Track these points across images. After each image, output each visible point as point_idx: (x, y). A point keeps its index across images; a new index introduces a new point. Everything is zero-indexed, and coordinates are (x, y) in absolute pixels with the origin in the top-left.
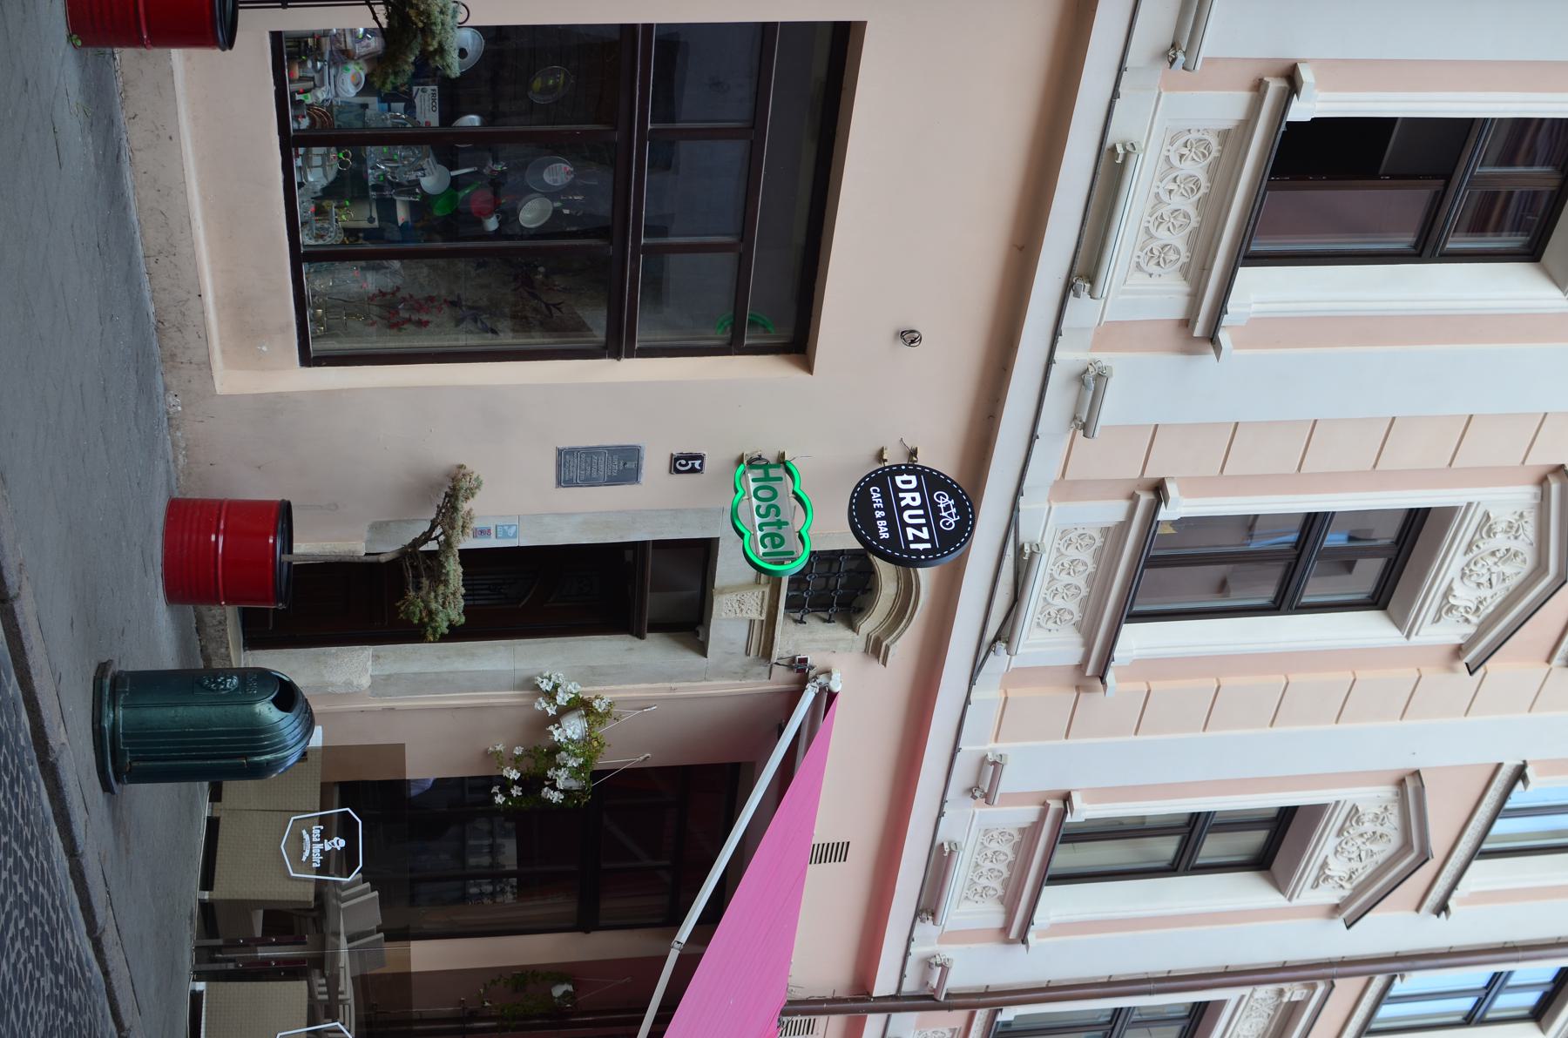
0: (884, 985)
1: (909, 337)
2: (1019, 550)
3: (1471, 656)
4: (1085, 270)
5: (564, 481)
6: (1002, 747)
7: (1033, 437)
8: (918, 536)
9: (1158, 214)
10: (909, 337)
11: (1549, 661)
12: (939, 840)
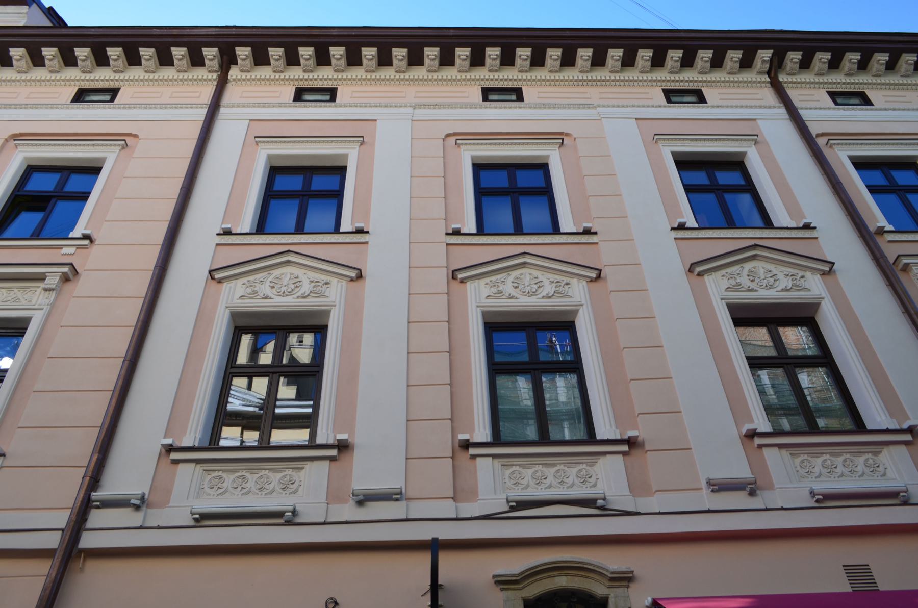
2: (513, 509)
4: (288, 518)
6: (704, 484)
7: (767, 509)
9: (257, 491)
11: (597, 243)
12: (192, 523)
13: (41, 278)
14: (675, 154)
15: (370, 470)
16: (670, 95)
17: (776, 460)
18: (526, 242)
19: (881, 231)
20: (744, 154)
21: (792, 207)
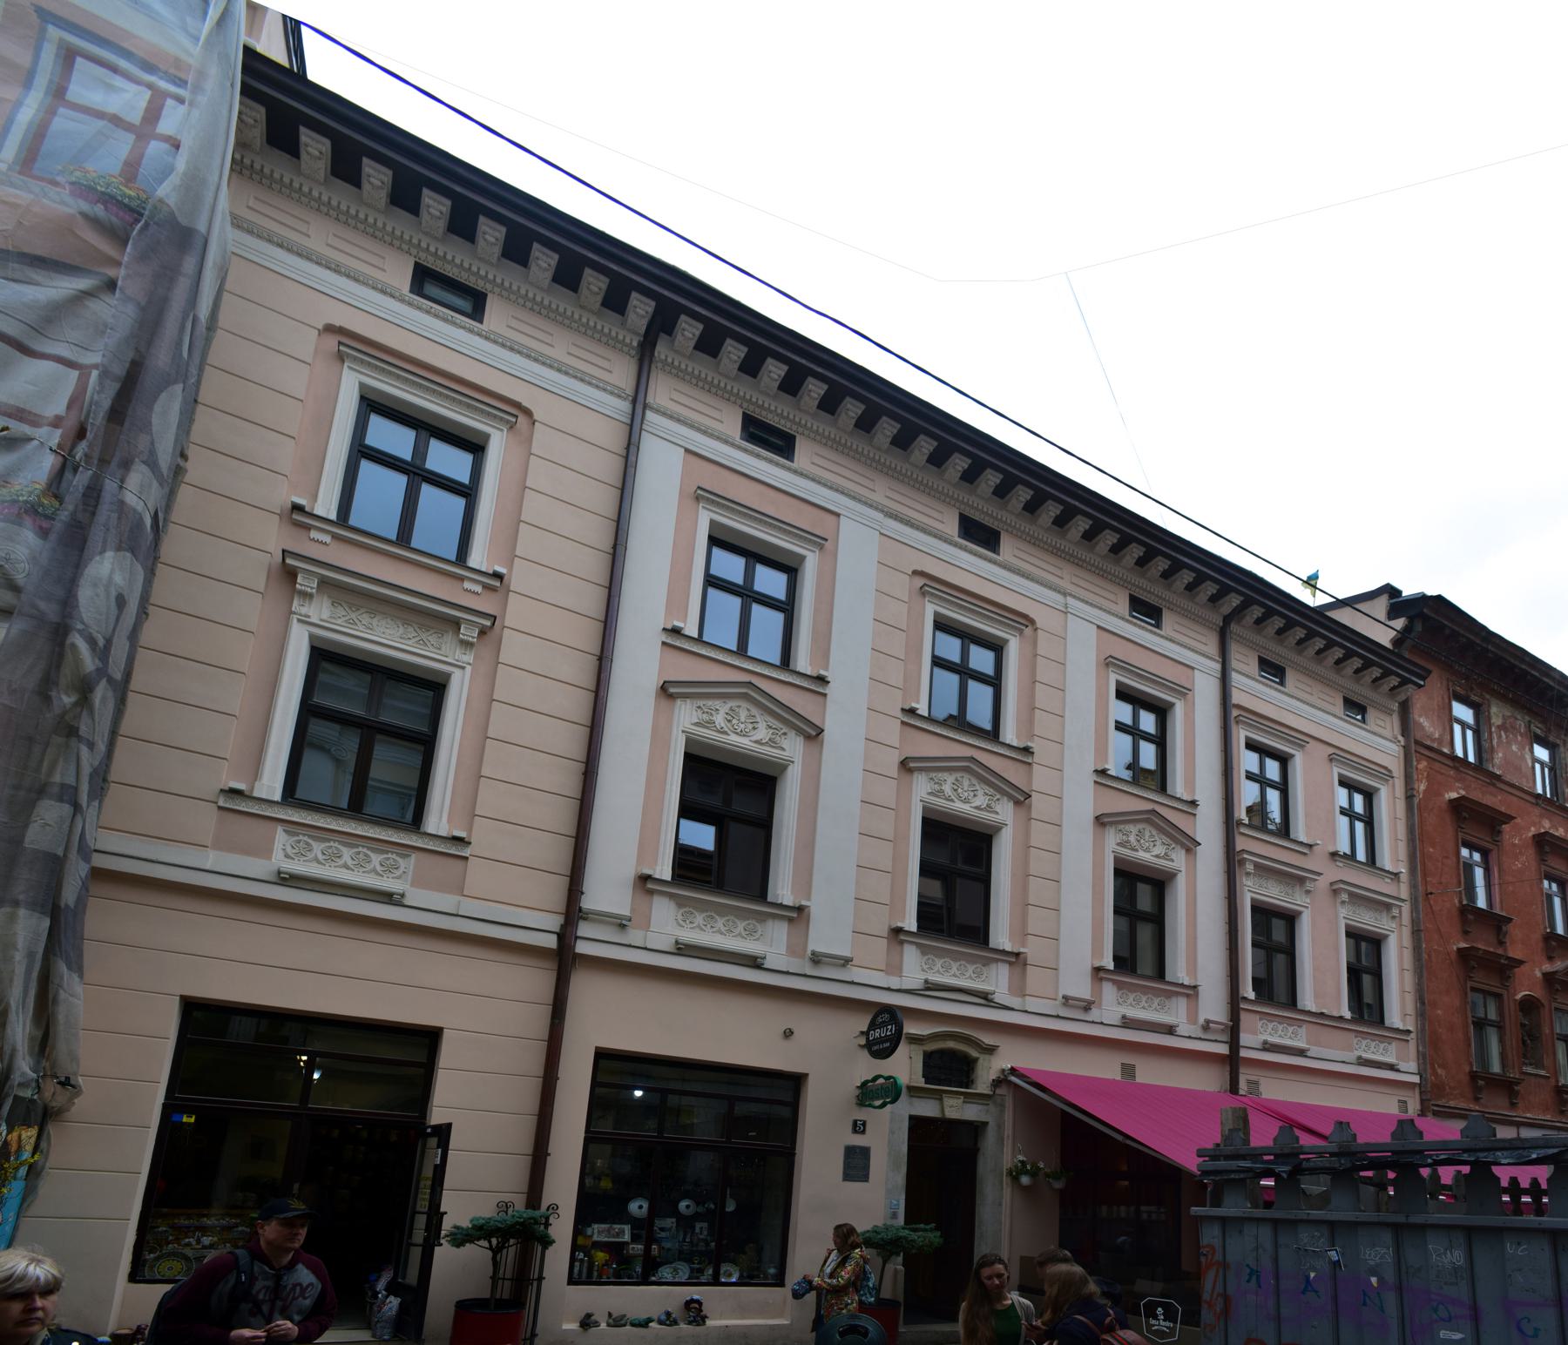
0: (1223, 1049)
1: (788, 1034)
3: (1021, 799)
5: (865, 1178)
8: (890, 1030)
10: (788, 1034)
13: (456, 624)
14: (936, 614)
15: (827, 935)
16: (425, 279)
17: (1109, 991)
18: (983, 745)
19: (1240, 823)
20: (1377, 790)
21: (1190, 782)
